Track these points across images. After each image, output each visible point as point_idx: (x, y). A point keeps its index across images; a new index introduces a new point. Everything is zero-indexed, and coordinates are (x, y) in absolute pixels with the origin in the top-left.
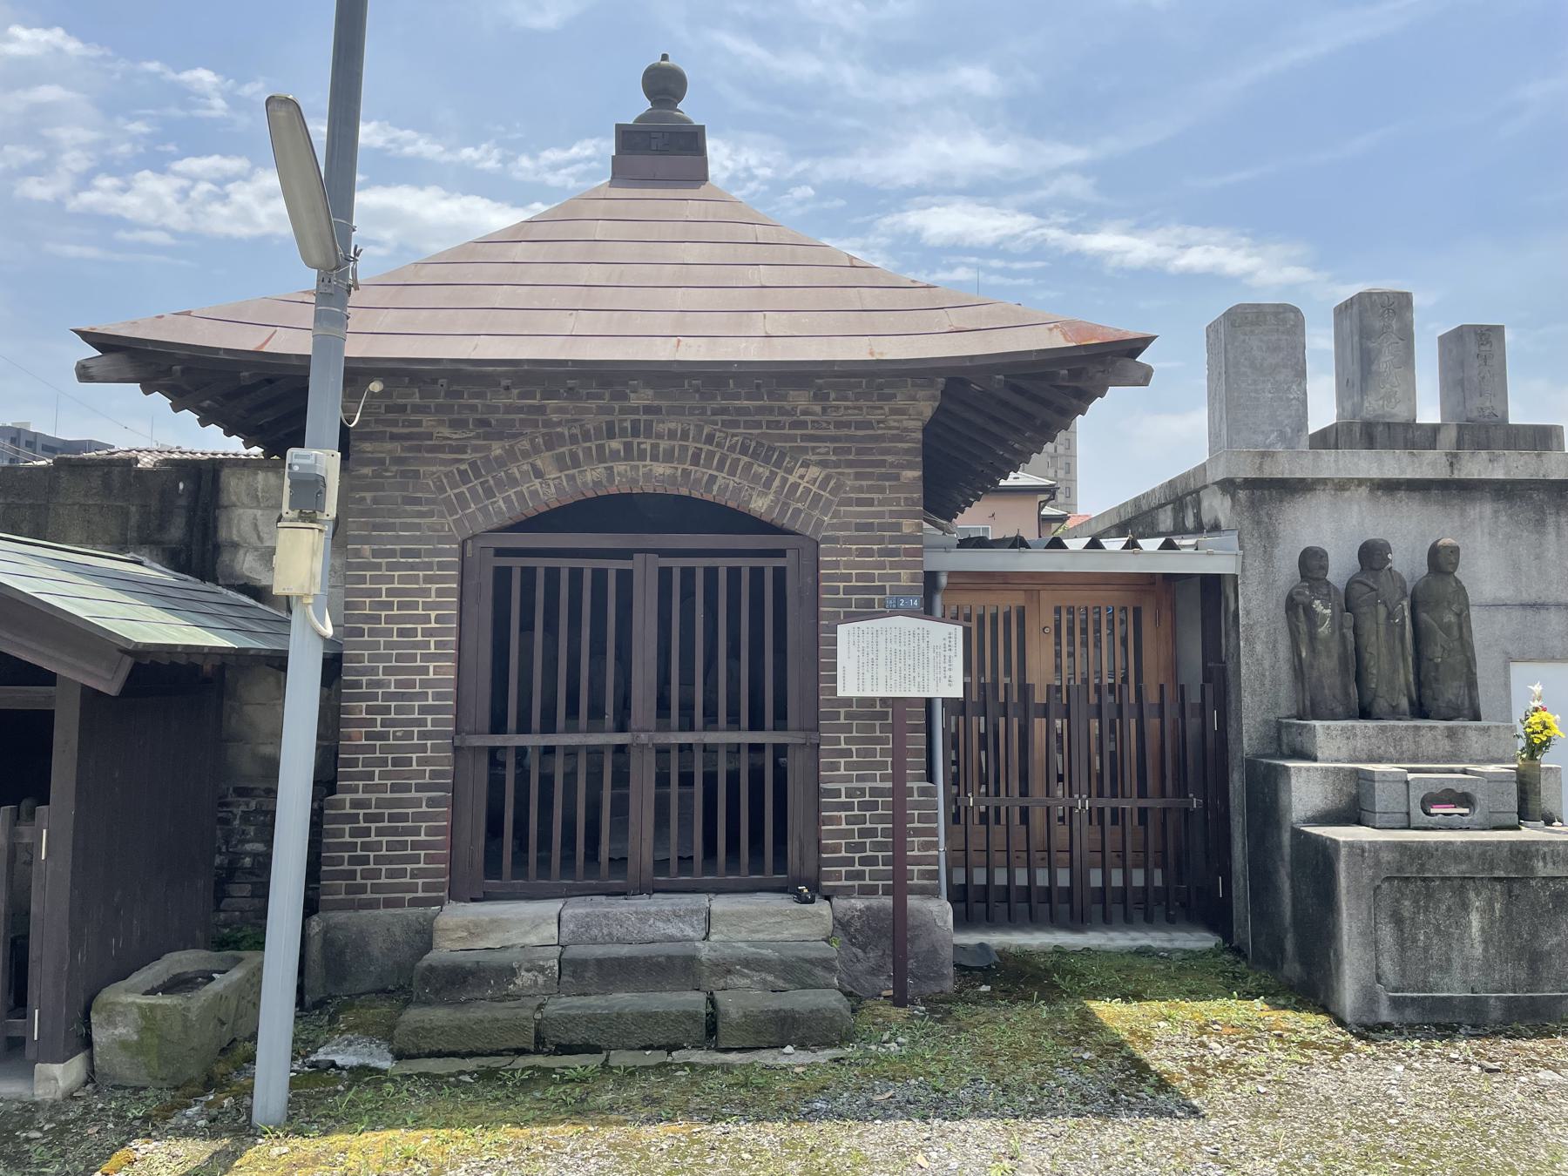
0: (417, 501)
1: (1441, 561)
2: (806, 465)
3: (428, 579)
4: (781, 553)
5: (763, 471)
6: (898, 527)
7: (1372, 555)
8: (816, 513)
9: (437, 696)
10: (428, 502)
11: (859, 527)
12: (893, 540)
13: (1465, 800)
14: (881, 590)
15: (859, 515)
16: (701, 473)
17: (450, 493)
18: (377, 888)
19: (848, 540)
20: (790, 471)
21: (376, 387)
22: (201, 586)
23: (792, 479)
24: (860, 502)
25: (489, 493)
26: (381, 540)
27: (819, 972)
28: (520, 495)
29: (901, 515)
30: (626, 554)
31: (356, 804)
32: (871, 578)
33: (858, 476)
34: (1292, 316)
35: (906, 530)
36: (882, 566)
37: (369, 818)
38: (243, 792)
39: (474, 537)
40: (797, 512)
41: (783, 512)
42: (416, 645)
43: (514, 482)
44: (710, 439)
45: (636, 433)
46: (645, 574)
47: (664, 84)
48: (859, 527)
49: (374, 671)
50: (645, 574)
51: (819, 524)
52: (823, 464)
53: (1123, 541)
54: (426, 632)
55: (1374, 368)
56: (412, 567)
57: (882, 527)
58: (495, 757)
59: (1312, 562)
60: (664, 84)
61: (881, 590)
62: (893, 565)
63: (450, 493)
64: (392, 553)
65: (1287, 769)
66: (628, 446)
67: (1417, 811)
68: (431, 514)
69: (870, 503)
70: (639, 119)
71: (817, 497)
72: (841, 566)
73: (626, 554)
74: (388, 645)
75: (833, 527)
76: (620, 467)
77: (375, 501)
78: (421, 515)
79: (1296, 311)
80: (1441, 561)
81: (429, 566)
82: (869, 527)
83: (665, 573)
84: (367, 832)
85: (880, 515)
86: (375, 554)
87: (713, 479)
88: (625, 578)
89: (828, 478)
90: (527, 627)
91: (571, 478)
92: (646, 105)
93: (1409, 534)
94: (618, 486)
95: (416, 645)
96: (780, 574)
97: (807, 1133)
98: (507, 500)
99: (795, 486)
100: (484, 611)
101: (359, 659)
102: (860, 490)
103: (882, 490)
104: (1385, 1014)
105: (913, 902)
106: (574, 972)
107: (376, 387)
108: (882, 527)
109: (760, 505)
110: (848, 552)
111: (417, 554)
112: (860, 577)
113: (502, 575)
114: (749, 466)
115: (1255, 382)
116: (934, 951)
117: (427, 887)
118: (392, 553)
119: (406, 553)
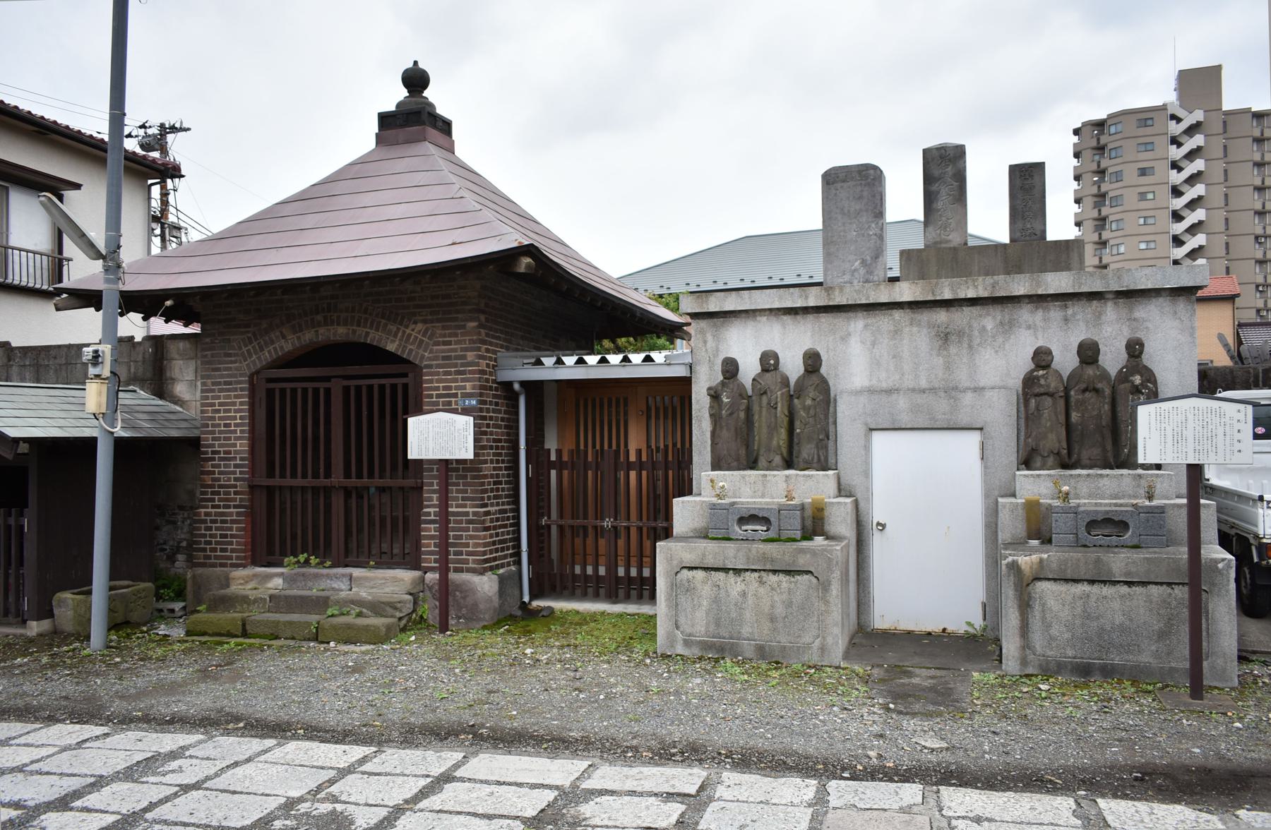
0: (230, 355)
1: (813, 361)
2: (415, 323)
3: (236, 397)
4: (405, 375)
5: (393, 328)
6: (464, 357)
7: (769, 362)
8: (421, 352)
9: (241, 459)
10: (236, 355)
11: (444, 358)
12: (463, 365)
13: (766, 521)
14: (455, 395)
15: (443, 351)
16: (361, 331)
17: (244, 349)
18: (216, 557)
19: (439, 366)
20: (407, 327)
21: (168, 303)
22: (161, 402)
23: (408, 331)
24: (445, 343)
25: (262, 349)
26: (215, 377)
27: (388, 609)
28: (275, 349)
29: (466, 350)
30: (328, 379)
31: (207, 514)
32: (450, 388)
33: (444, 328)
34: (872, 172)
35: (469, 359)
36: (456, 381)
37: (212, 522)
38: (181, 508)
39: (257, 372)
40: (411, 350)
41: (403, 351)
42: (231, 432)
43: (272, 342)
44: (365, 312)
45: (329, 311)
46: (337, 387)
47: (416, 80)
48: (444, 358)
49: (213, 446)
50: (337, 387)
51: (423, 357)
52: (425, 322)
53: (620, 357)
54: (236, 425)
55: (934, 206)
56: (229, 390)
57: (457, 358)
58: (270, 490)
59: (730, 368)
60: (416, 80)
61: (455, 395)
62: (463, 380)
63: (244, 349)
64: (219, 383)
65: (22, 504)
66: (325, 318)
67: (1082, 532)
68: (235, 362)
69: (449, 343)
70: (398, 105)
71: (421, 341)
72: (433, 383)
73: (328, 379)
74: (220, 432)
75: (430, 359)
76: (322, 330)
77: (212, 356)
78: (232, 362)
79: (875, 168)
80: (813, 361)
81: (235, 390)
82: (448, 358)
83: (346, 390)
84: (210, 528)
85: (455, 350)
86: (213, 384)
87: (367, 334)
88: (328, 392)
89: (427, 330)
90: (382, 416)
91: (299, 338)
92: (404, 93)
93: (791, 344)
94: (352, 338)
95: (231, 432)
96: (405, 386)
97: (1136, 803)
98: (269, 352)
99: (410, 335)
100: (262, 414)
101: (207, 439)
102: (444, 336)
103: (456, 335)
104: (680, 649)
105: (452, 576)
106: (278, 602)
107: (168, 303)
108: (457, 358)
109: (391, 347)
110: (438, 374)
111: (230, 383)
112: (445, 388)
113: (270, 393)
114: (386, 325)
115: (844, 224)
116: (476, 605)
117: (237, 558)
118: (219, 383)
119: (226, 383)
